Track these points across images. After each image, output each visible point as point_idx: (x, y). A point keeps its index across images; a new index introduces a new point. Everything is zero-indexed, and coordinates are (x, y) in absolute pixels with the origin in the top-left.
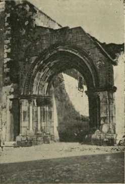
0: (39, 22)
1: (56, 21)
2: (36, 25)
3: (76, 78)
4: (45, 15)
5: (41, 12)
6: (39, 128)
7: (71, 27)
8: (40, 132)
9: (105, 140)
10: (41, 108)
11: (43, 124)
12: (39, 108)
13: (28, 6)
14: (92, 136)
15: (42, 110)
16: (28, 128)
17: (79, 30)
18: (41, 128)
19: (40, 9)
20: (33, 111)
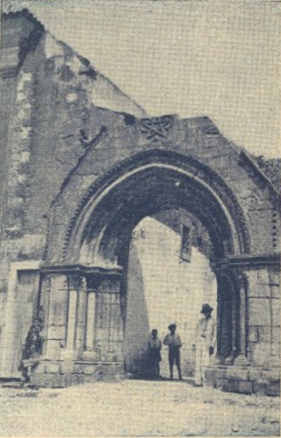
0: (98, 98)
1: (132, 98)
2: (92, 105)
3: (175, 227)
4: (110, 82)
5: (102, 76)
6: (90, 343)
7: (183, 116)
8: (89, 354)
9: (260, 381)
10: (97, 296)
11: (101, 334)
12: (92, 295)
13: (76, 60)
14: (229, 371)
15: (100, 301)
16: (62, 342)
17: (206, 126)
18: (95, 342)
19: (102, 72)
20: (77, 305)
